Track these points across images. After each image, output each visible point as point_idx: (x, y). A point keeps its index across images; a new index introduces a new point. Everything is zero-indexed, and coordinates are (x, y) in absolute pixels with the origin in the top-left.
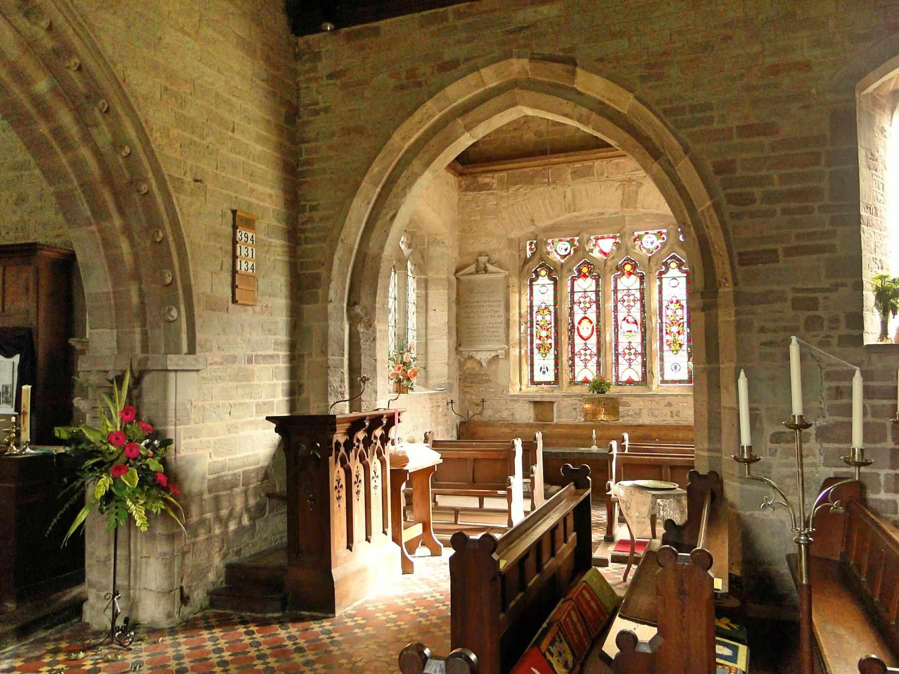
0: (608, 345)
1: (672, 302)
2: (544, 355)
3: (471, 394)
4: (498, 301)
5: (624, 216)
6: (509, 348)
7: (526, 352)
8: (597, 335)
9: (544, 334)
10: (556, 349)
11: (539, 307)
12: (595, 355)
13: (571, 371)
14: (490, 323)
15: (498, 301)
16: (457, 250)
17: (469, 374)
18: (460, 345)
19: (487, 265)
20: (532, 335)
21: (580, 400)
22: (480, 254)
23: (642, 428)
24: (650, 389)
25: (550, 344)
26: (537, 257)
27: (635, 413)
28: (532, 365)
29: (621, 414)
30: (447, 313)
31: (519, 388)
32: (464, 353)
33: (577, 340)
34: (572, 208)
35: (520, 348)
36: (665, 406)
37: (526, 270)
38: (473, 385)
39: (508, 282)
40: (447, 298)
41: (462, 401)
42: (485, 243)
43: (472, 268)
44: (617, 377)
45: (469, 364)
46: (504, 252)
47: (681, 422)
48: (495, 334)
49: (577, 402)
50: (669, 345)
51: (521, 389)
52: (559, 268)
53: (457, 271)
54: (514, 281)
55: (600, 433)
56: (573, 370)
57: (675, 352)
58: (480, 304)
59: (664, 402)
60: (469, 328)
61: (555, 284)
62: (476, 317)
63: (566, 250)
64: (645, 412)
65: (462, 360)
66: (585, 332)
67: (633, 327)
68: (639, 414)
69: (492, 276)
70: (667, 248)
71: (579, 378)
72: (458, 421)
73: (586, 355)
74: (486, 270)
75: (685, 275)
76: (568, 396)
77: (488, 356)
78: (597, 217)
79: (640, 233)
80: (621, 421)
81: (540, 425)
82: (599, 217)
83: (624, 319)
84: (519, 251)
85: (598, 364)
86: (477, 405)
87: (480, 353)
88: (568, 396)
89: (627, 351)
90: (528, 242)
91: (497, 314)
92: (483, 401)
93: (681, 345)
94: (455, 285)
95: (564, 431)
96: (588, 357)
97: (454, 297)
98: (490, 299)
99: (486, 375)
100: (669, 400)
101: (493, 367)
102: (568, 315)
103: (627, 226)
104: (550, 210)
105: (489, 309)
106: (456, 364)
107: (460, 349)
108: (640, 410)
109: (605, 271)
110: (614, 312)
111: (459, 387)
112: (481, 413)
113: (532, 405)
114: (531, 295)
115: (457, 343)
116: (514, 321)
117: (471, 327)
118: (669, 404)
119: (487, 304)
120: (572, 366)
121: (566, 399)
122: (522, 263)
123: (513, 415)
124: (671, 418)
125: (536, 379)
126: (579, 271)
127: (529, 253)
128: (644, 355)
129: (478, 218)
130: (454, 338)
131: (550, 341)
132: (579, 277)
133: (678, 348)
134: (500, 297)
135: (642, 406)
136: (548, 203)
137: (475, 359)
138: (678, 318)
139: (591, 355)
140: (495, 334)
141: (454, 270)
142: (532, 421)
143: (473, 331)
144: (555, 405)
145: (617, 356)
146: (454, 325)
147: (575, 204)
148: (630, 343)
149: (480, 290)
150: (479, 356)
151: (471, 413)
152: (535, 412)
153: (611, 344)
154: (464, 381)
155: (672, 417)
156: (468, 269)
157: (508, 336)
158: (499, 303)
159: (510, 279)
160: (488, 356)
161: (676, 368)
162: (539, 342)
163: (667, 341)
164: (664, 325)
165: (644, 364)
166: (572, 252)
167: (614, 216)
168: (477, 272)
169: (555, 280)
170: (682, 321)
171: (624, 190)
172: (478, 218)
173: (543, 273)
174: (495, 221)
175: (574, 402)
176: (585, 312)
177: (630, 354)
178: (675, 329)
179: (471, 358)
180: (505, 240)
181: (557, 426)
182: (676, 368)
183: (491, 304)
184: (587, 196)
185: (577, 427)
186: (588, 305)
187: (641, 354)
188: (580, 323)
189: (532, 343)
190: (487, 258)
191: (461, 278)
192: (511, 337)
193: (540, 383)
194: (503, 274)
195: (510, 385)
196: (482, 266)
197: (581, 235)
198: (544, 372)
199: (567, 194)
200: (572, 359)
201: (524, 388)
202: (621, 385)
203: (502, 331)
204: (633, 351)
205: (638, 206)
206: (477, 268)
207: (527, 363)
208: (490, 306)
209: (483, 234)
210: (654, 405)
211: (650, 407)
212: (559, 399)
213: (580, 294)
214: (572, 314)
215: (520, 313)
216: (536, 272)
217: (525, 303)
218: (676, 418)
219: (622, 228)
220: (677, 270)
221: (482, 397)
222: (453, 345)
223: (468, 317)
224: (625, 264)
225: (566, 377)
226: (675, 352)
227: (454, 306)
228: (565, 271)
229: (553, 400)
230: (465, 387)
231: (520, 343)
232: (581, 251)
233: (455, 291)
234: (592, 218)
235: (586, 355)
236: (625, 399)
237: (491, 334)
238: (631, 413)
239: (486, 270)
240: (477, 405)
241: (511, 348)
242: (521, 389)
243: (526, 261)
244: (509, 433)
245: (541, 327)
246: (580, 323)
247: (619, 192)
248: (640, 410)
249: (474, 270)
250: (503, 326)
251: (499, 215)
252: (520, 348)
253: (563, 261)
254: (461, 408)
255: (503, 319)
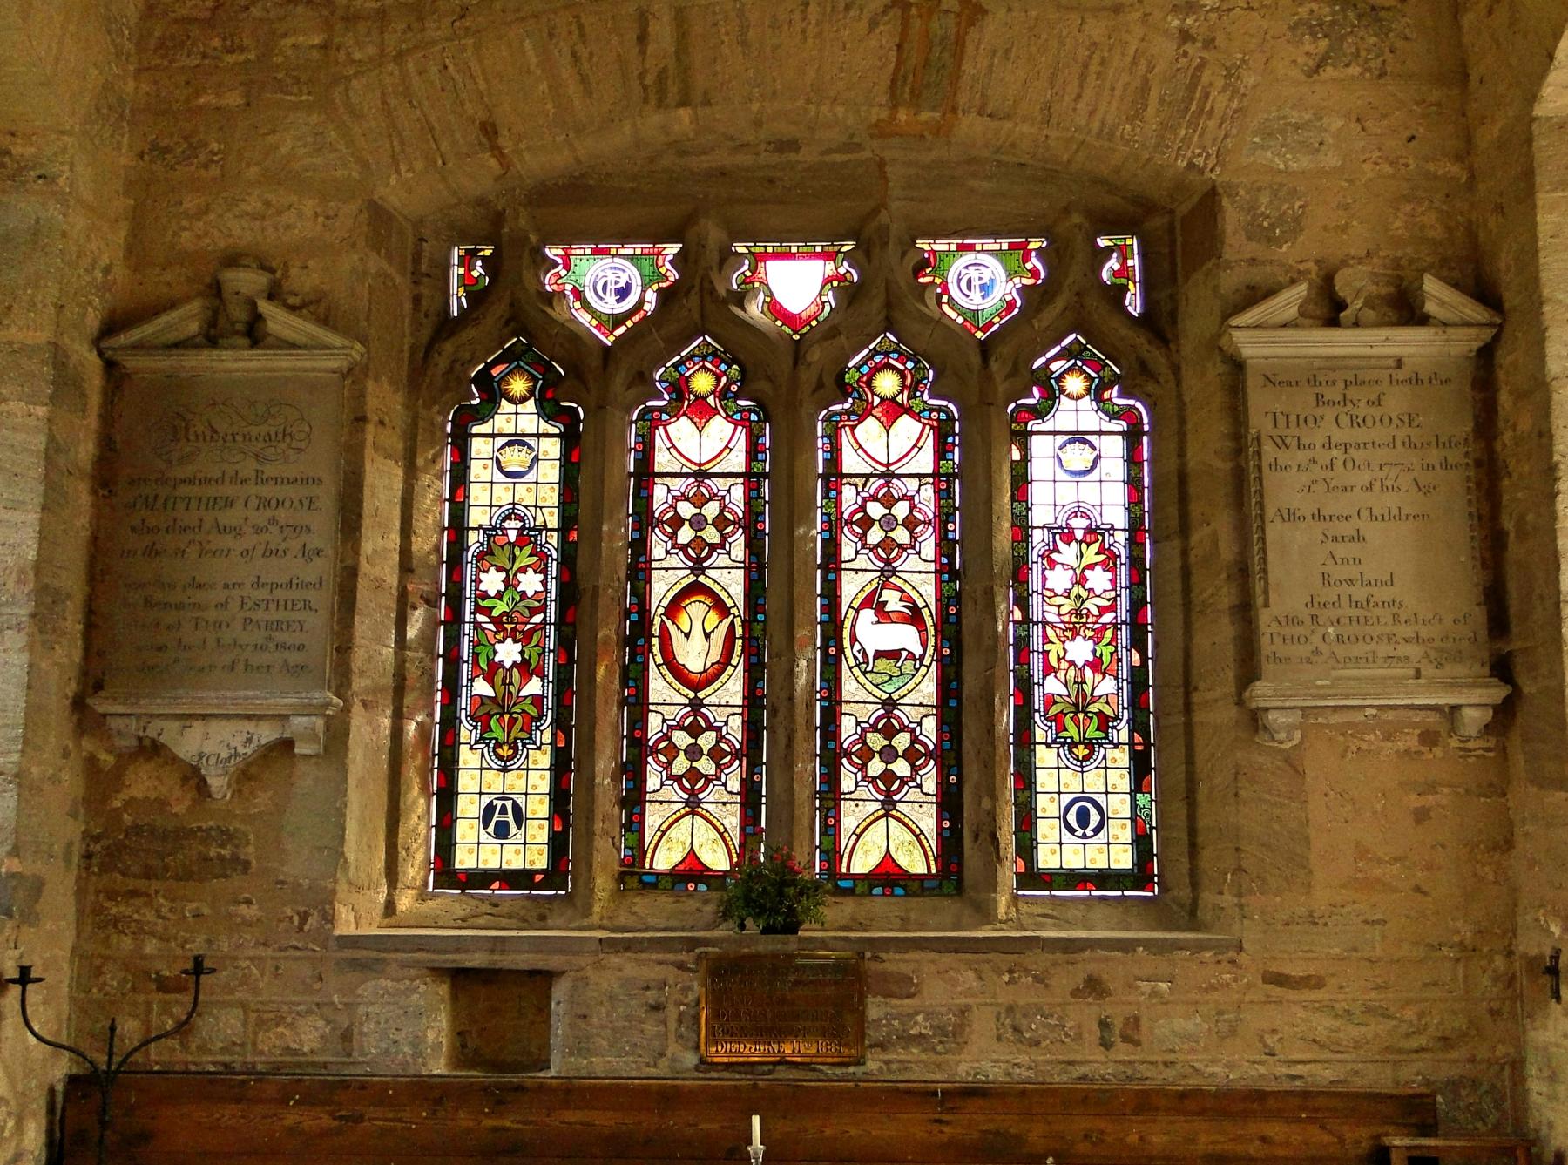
0: (800, 710)
1: (1069, 537)
2: (505, 751)
3: (140, 932)
4: (305, 481)
5: (881, 164)
6: (346, 710)
7: (424, 732)
8: (748, 668)
9: (508, 653)
10: (560, 724)
11: (492, 532)
12: (736, 755)
13: (628, 826)
14: (258, 584)
15: (305, 481)
16: (121, 235)
17: (136, 829)
18: (99, 687)
19: (264, 307)
20: (453, 660)
21: (681, 966)
22: (232, 260)
23: (972, 1104)
24: (985, 913)
25: (538, 700)
26: (498, 310)
27: (940, 1030)
28: (448, 796)
29: (873, 1034)
30: (33, 517)
31: (382, 898)
32: (114, 723)
33: (660, 687)
34: (673, 89)
35: (398, 717)
36: (1076, 993)
37: (441, 362)
38: (155, 885)
39: (361, 396)
40: (40, 441)
41: (89, 967)
42: (255, 217)
43: (187, 319)
44: (833, 855)
45: (142, 783)
46: (348, 262)
47: (1146, 1071)
48: (280, 637)
49: (670, 974)
50: (1058, 720)
51: (390, 907)
52: (595, 362)
53: (110, 327)
54: (385, 399)
55: (782, 1127)
56: (635, 824)
57: (1082, 751)
58: (211, 491)
59: (1066, 979)
60: (148, 603)
61: (570, 440)
62: (193, 552)
63: (623, 293)
64: (982, 1025)
65: (107, 759)
66: (694, 654)
67: (905, 637)
68: (954, 1032)
69: (284, 363)
70: (1060, 303)
71: (665, 859)
72: (60, 1069)
73: (694, 752)
74: (254, 334)
75: (1121, 426)
76: (628, 946)
77: (237, 742)
78: (765, 158)
79: (940, 246)
80: (872, 1065)
81: (486, 1089)
82: (775, 159)
83: (867, 603)
84: (417, 278)
85: (749, 798)
86: (163, 985)
87: (198, 726)
88: (628, 946)
89: (876, 741)
90: (456, 254)
91: (295, 545)
92: (198, 968)
93: (1105, 722)
94: (95, 400)
95: (605, 1120)
96: (705, 766)
97: (86, 451)
98: (269, 470)
99: (227, 836)
100: (1092, 968)
101: (263, 800)
102: (623, 573)
103: (895, 205)
104: (573, 89)
105: (261, 518)
106: (71, 782)
107: (101, 705)
108: (964, 1011)
109: (794, 381)
110: (825, 567)
111: (80, 892)
112: (183, 1028)
113: (444, 989)
114: (461, 477)
115: (84, 673)
116: (379, 584)
117: (159, 596)
118: (1094, 987)
119: (253, 490)
120: (635, 801)
121: (615, 960)
122: (426, 334)
123: (346, 1036)
124: (1098, 1055)
125: (464, 859)
126: (680, 388)
127: (457, 300)
128: (948, 756)
129: (234, 99)
130: (69, 652)
131: (534, 687)
132: (675, 412)
133: (1092, 732)
134: (319, 461)
135: (968, 993)
136: (566, 58)
137: (175, 759)
138: (1091, 605)
139: (716, 754)
140: (280, 637)
141: (93, 321)
142: (439, 1067)
143: (170, 617)
144: (560, 990)
145: (833, 759)
146: (72, 582)
147: (685, 72)
148: (890, 704)
149: (223, 427)
150: (189, 743)
151: (130, 1029)
152: (455, 1018)
153: (810, 706)
154: (104, 869)
155: (1106, 1045)
156: (163, 319)
157: (344, 648)
158: (316, 490)
159: (371, 385)
160: (237, 742)
161: (1083, 817)
162: (482, 688)
163: (1050, 700)
164: (1036, 632)
165: (948, 803)
166: (229, 796)
167: (838, 158)
168: (211, 338)
169: (567, 419)
170: (1108, 618)
171: (905, 23)
172: (234, 99)
173: (518, 386)
174: (314, 118)
175: (653, 973)
176: (698, 567)
177: (889, 754)
178: (1080, 650)
179: (152, 750)
180: (352, 207)
181: (570, 1093)
182: (1083, 817)
183: (266, 491)
184: (744, 43)
185: (667, 1097)
186: (711, 535)
187: (937, 755)
188: (674, 609)
189: (452, 688)
190: (263, 280)
191: (131, 363)
192: (359, 657)
193: (481, 878)
194: (337, 354)
195: (342, 887)
196: (239, 314)
197: (691, 234)
198: (502, 831)
199: (653, 27)
200: (634, 771)
201: (405, 902)
202: (850, 892)
203: (317, 624)
204: (902, 741)
205: (962, 100)
206: (212, 323)
207: (425, 788)
208: (264, 503)
209: (253, 172)
210: (1026, 994)
211: (1004, 999)
212: (582, 961)
213: (678, 485)
214: (640, 572)
215: (405, 552)
216: (484, 380)
217: (433, 513)
218: (1122, 1052)
219: (875, 211)
220: (1087, 403)
221: (197, 946)
222: (61, 683)
223: (152, 552)
224: (878, 369)
225: (607, 854)
226: (1082, 751)
227: (82, 495)
228: (619, 379)
229: (553, 962)
230: (112, 895)
231: (399, 690)
232: (694, 299)
233: (93, 421)
234: (744, 159)
235: (694, 752)
236: (894, 963)
237: (259, 636)
238: (921, 1026)
239: (254, 334)
240: (163, 985)
241: (357, 709)
242: (390, 907)
243: (446, 327)
244: (325, 1133)
245: (497, 621)
246: (674, 609)
247: (887, 34)
248: (964, 1011)
249: (194, 327)
250: (323, 599)
251: (337, 94)
252: (398, 717)
253: (608, 341)
254: (82, 1007)
255: (323, 567)
